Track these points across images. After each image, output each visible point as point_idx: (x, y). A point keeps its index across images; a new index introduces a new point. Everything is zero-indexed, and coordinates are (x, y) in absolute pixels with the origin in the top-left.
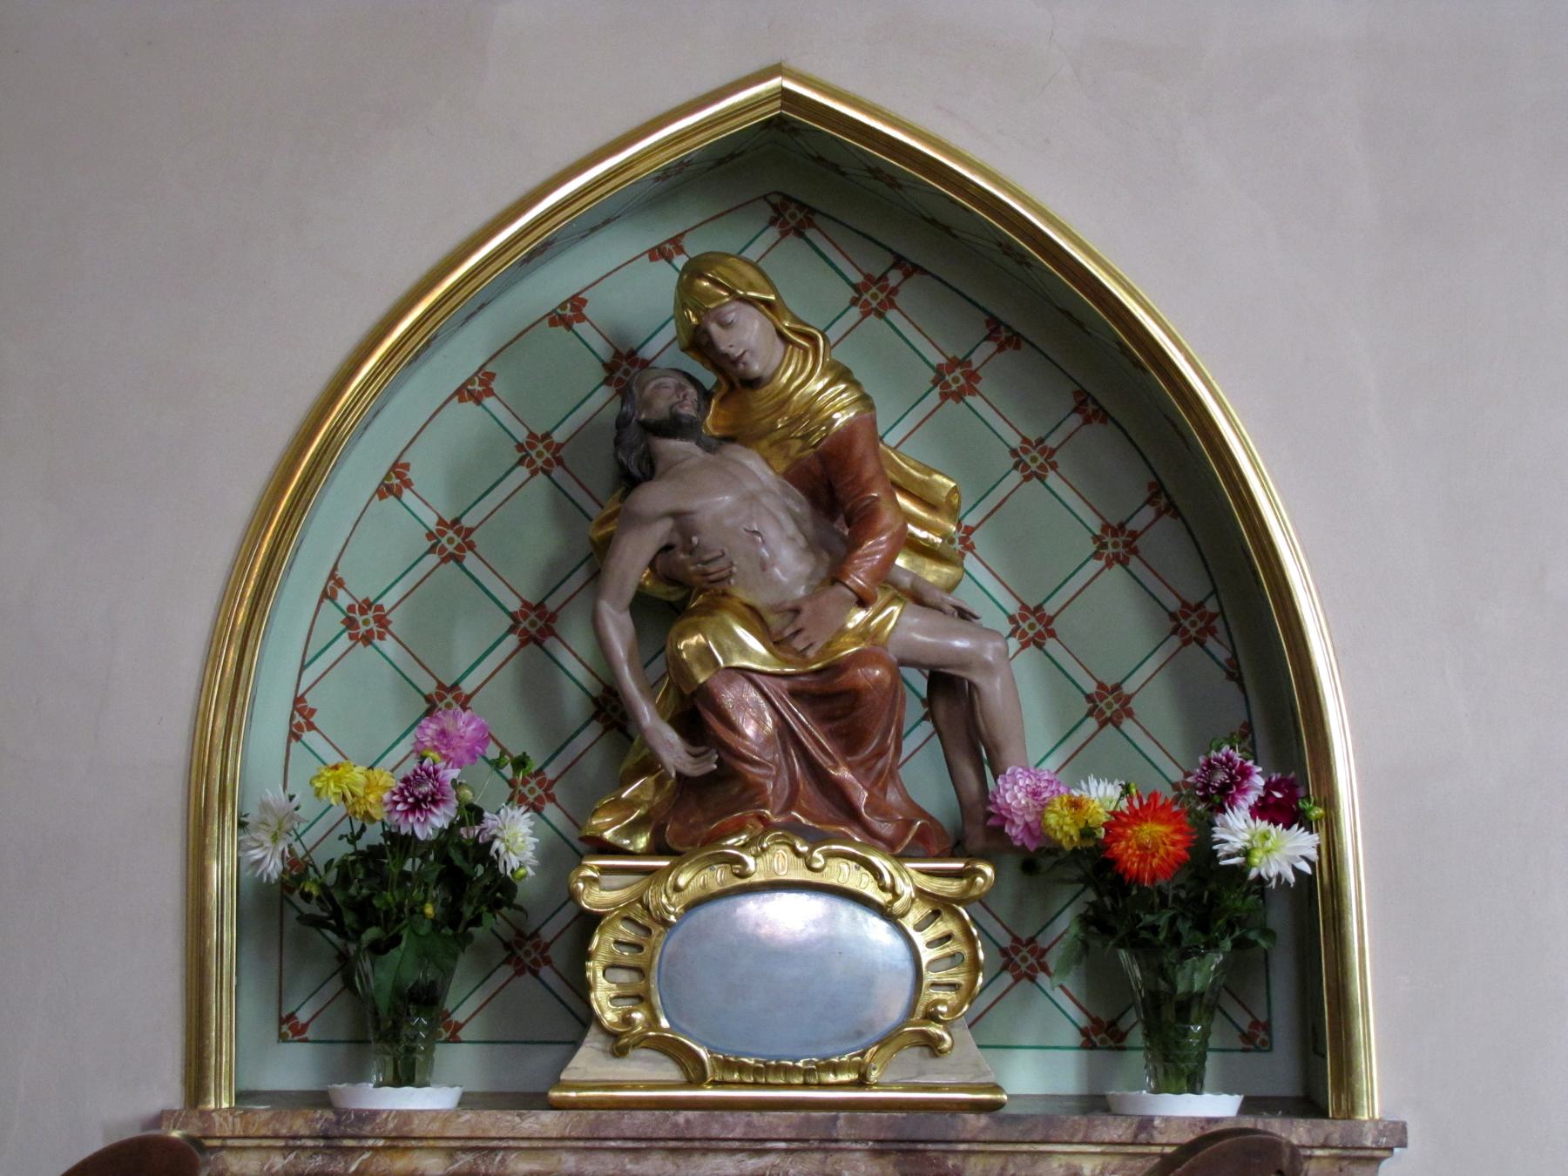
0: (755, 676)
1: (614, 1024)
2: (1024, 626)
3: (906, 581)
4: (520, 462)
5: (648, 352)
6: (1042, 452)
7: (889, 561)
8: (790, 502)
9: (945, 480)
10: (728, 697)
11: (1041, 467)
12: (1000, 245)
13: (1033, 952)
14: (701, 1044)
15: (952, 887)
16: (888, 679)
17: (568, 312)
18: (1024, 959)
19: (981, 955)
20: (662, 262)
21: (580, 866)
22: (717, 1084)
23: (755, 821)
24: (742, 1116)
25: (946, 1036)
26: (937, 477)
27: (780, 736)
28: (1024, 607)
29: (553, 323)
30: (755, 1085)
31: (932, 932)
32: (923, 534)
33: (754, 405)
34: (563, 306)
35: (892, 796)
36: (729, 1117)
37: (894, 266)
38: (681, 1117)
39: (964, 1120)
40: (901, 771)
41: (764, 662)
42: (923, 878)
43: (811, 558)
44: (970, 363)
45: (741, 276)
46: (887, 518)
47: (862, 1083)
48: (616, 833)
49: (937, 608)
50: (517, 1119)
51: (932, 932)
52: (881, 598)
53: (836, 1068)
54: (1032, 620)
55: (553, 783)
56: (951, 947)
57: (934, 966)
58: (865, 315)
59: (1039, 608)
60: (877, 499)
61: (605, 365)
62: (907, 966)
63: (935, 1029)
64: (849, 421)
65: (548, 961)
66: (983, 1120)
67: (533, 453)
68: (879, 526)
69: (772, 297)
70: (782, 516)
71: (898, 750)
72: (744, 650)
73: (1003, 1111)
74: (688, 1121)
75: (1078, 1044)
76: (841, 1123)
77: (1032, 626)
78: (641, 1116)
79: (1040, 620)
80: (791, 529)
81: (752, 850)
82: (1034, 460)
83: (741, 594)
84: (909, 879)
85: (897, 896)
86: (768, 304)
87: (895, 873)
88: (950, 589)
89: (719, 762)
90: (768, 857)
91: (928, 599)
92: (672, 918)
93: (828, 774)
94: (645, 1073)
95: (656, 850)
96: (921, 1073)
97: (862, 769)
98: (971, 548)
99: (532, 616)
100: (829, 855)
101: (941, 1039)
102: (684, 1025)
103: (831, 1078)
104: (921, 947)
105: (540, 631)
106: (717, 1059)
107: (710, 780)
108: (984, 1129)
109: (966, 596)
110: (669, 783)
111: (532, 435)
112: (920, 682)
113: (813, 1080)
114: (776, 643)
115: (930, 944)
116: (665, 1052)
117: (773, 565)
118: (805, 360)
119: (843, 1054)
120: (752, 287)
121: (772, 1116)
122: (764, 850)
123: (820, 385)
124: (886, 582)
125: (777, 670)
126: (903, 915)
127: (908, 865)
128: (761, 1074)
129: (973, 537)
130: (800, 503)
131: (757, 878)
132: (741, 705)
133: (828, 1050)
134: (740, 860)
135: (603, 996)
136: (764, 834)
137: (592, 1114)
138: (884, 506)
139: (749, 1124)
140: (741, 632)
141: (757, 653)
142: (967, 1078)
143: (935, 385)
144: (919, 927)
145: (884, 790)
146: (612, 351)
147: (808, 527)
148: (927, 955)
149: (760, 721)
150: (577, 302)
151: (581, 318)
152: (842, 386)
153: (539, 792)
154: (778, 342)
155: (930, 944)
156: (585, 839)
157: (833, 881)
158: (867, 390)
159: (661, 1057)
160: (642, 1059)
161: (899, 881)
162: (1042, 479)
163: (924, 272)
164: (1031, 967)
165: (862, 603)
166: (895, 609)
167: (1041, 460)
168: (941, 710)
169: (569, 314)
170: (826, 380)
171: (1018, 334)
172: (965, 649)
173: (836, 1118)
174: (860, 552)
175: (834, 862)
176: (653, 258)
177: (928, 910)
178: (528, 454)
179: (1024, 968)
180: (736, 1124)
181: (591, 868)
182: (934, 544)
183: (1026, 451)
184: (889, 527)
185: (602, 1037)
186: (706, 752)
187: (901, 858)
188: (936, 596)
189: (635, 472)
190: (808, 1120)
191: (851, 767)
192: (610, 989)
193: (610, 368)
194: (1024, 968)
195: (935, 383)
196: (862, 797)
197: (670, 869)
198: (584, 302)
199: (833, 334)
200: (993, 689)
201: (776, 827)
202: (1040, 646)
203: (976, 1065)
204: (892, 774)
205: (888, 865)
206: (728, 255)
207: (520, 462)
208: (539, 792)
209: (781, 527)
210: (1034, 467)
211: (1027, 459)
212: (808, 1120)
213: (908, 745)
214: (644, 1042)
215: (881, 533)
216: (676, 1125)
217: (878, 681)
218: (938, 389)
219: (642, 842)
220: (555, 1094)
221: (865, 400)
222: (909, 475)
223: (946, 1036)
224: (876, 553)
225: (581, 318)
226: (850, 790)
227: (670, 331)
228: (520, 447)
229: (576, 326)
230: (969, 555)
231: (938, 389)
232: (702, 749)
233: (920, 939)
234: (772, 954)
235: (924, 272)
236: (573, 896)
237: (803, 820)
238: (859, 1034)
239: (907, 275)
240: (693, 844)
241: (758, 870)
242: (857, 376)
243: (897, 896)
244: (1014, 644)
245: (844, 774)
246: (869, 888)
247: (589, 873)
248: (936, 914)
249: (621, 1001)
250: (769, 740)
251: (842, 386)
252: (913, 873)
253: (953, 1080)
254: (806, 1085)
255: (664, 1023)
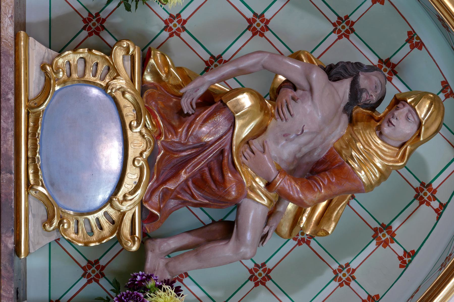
0: (231, 131)
1: (57, 62)
2: (260, 271)
3: (280, 209)
4: (339, 18)
5: (395, 80)
6: (348, 279)
7: (291, 199)
8: (319, 150)
9: (332, 228)
10: (220, 119)
11: (340, 279)
12: (450, 255)
13: (97, 276)
14: (47, 106)
15: (126, 230)
16: (230, 198)
17: (415, 41)
18: (93, 272)
19: (92, 245)
20: (441, 88)
21: (135, 44)
22: (28, 113)
23: (158, 132)
24: (11, 126)
25: (52, 228)
26: (333, 225)
27: (202, 146)
28: (270, 271)
29: (409, 33)
30: (27, 133)
31: (103, 221)
32: (304, 219)
33: (368, 132)
34: (418, 38)
35: (172, 203)
36: (11, 120)
37: (441, 204)
38: (11, 96)
39: (10, 237)
40: (185, 208)
41: (238, 136)
42: (131, 216)
43: (291, 159)
44: (392, 242)
45: (432, 124)
46: (311, 197)
47: (29, 186)
48: (153, 65)
49: (267, 224)
50: (10, 16)
51: (103, 221)
52: (272, 195)
53: (36, 173)
54: (264, 275)
55: (179, 36)
56: (96, 230)
57: (87, 222)
58: (416, 190)
59: (270, 278)
60: (320, 192)
61: (388, 59)
62: (86, 208)
63: (55, 223)
64: (360, 178)
65: (90, 35)
66: (11, 246)
67: (344, 24)
68: (306, 193)
69: (421, 139)
70: (311, 145)
71: (196, 205)
72: (244, 126)
73: (17, 257)
74: (9, 99)
75: (52, 299)
76: (9, 175)
77: (260, 275)
78: (11, 76)
79: (264, 278)
80: (305, 150)
81: (144, 131)
82: (344, 275)
83: (272, 123)
84: (130, 208)
85: (121, 203)
86: (419, 135)
87: (133, 201)
88: (277, 232)
89: (188, 115)
90: (140, 138)
91: (271, 220)
92: (109, 91)
93: (182, 169)
94: (34, 81)
95: (144, 86)
96: (34, 216)
97: (184, 187)
98: (299, 244)
99: (262, 25)
100: (141, 168)
101: (51, 226)
102: (56, 97)
103: (31, 171)
104: (96, 215)
105: (255, 28)
106: (40, 114)
107: (180, 113)
108: (6, 246)
109: (273, 241)
110: (176, 91)
111: (353, 23)
112: (231, 218)
113: (30, 161)
114: (247, 141)
115: (98, 219)
116: (44, 88)
117: (286, 140)
118: (391, 157)
119: (43, 176)
120: (427, 129)
121: (11, 141)
122: (143, 136)
123: (379, 165)
124: (280, 198)
125: (234, 142)
126: (112, 206)
127: (137, 209)
128: (33, 135)
129: (304, 245)
130: (319, 155)
131: (129, 133)
132: (216, 125)
133: (45, 170)
134: (138, 124)
135: (70, 56)
136: (152, 136)
137: (12, 52)
138: (317, 196)
139: (8, 130)
140: (252, 125)
141: (242, 133)
142: (31, 239)
143: (381, 225)
144: (106, 214)
145: (176, 198)
146: (396, 63)
147: (307, 159)
148: (92, 218)
149: (209, 134)
150: (420, 45)
151: (412, 47)
152: (378, 176)
153: (174, 29)
154: (399, 143)
155: (98, 219)
156: (150, 50)
157: (128, 171)
158: (376, 189)
159: (41, 87)
160: (39, 80)
161: (129, 203)
162: (335, 279)
163: (438, 219)
164: (89, 275)
165: (269, 185)
166: (265, 202)
167: (344, 279)
168: (153, 85)
169: (414, 41)
170: (381, 167)
171: (407, 267)
172: (246, 237)
173: (11, 173)
174: (293, 183)
175: (138, 171)
176: (443, 83)
177: (115, 218)
178: (343, 21)
179: (89, 271)
180: (7, 123)
181: (134, 51)
182: (300, 223)
183: (348, 271)
184: (306, 198)
185: (51, 57)
186: (193, 108)
187: (142, 204)
188: (273, 223)
189: (334, 71)
190: (10, 159)
191: (186, 181)
192: (74, 61)
193: (387, 62)
194: (89, 271)
195: (383, 225)
196: (171, 186)
197: (134, 90)
198: (420, 49)
199: (404, 171)
200: (225, 250)
201: (155, 143)
202: (250, 279)
203: (38, 243)
204: (184, 203)
205: (137, 198)
206: (443, 117)
207: (339, 18)
208: (174, 29)
209: (306, 144)
210: (340, 275)
211: (345, 271)
212: (10, 159)
213: (197, 211)
214: (48, 80)
215: (303, 194)
216: (7, 94)
217: (229, 193)
218: (379, 226)
219: (148, 78)
220: (22, 34)
221: (371, 187)
222: (334, 211)
223: (52, 228)
224: (293, 191)
225: (412, 47)
226: (175, 180)
227: (404, 89)
228: (347, 17)
229: (408, 45)
230: (296, 242)
231: (379, 226)
232: (194, 106)
233: (100, 214)
234: (93, 145)
235: (438, 219)
236: (118, 41)
237: (159, 156)
238: (52, 185)
239: (436, 211)
240: (147, 102)
241: (134, 135)
242: (383, 184)
243: (121, 203)
244: (251, 265)
245: (184, 176)
246: (125, 189)
247: (131, 50)
248: (113, 222)
249: (68, 66)
250: (199, 139)
251: (378, 176)
252: (133, 211)
253: (31, 232)
254: (27, 158)
255: (57, 88)
